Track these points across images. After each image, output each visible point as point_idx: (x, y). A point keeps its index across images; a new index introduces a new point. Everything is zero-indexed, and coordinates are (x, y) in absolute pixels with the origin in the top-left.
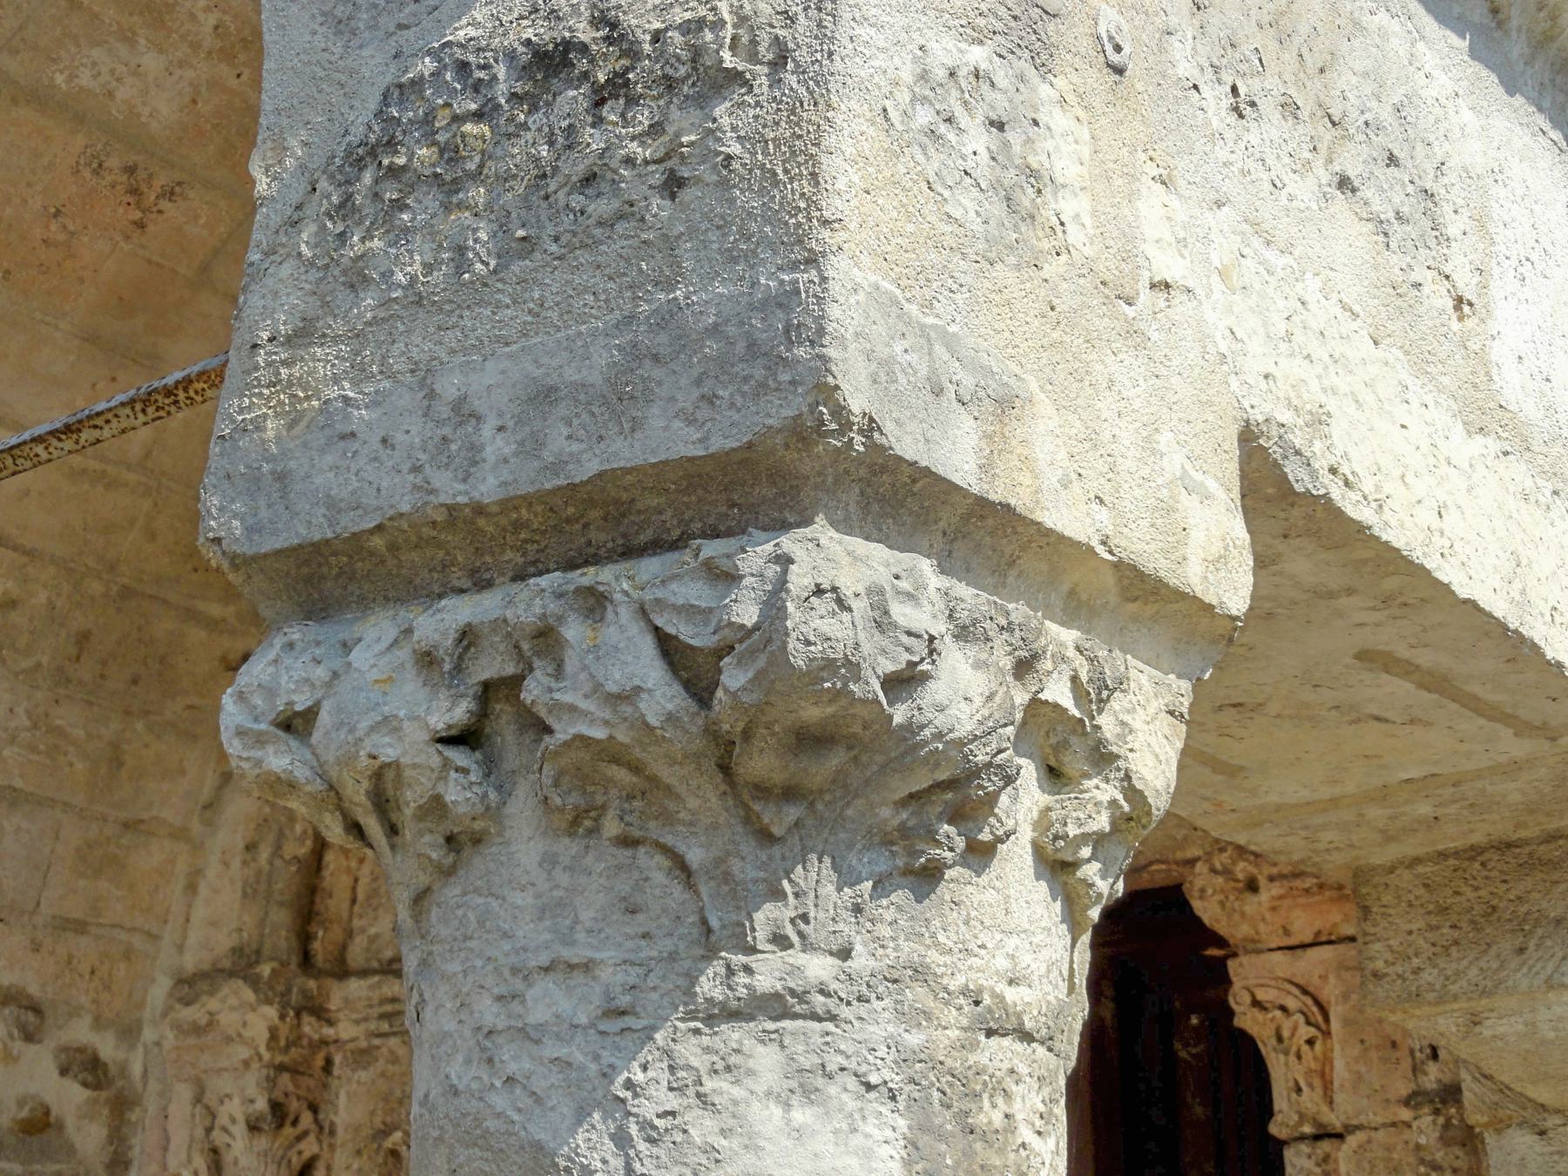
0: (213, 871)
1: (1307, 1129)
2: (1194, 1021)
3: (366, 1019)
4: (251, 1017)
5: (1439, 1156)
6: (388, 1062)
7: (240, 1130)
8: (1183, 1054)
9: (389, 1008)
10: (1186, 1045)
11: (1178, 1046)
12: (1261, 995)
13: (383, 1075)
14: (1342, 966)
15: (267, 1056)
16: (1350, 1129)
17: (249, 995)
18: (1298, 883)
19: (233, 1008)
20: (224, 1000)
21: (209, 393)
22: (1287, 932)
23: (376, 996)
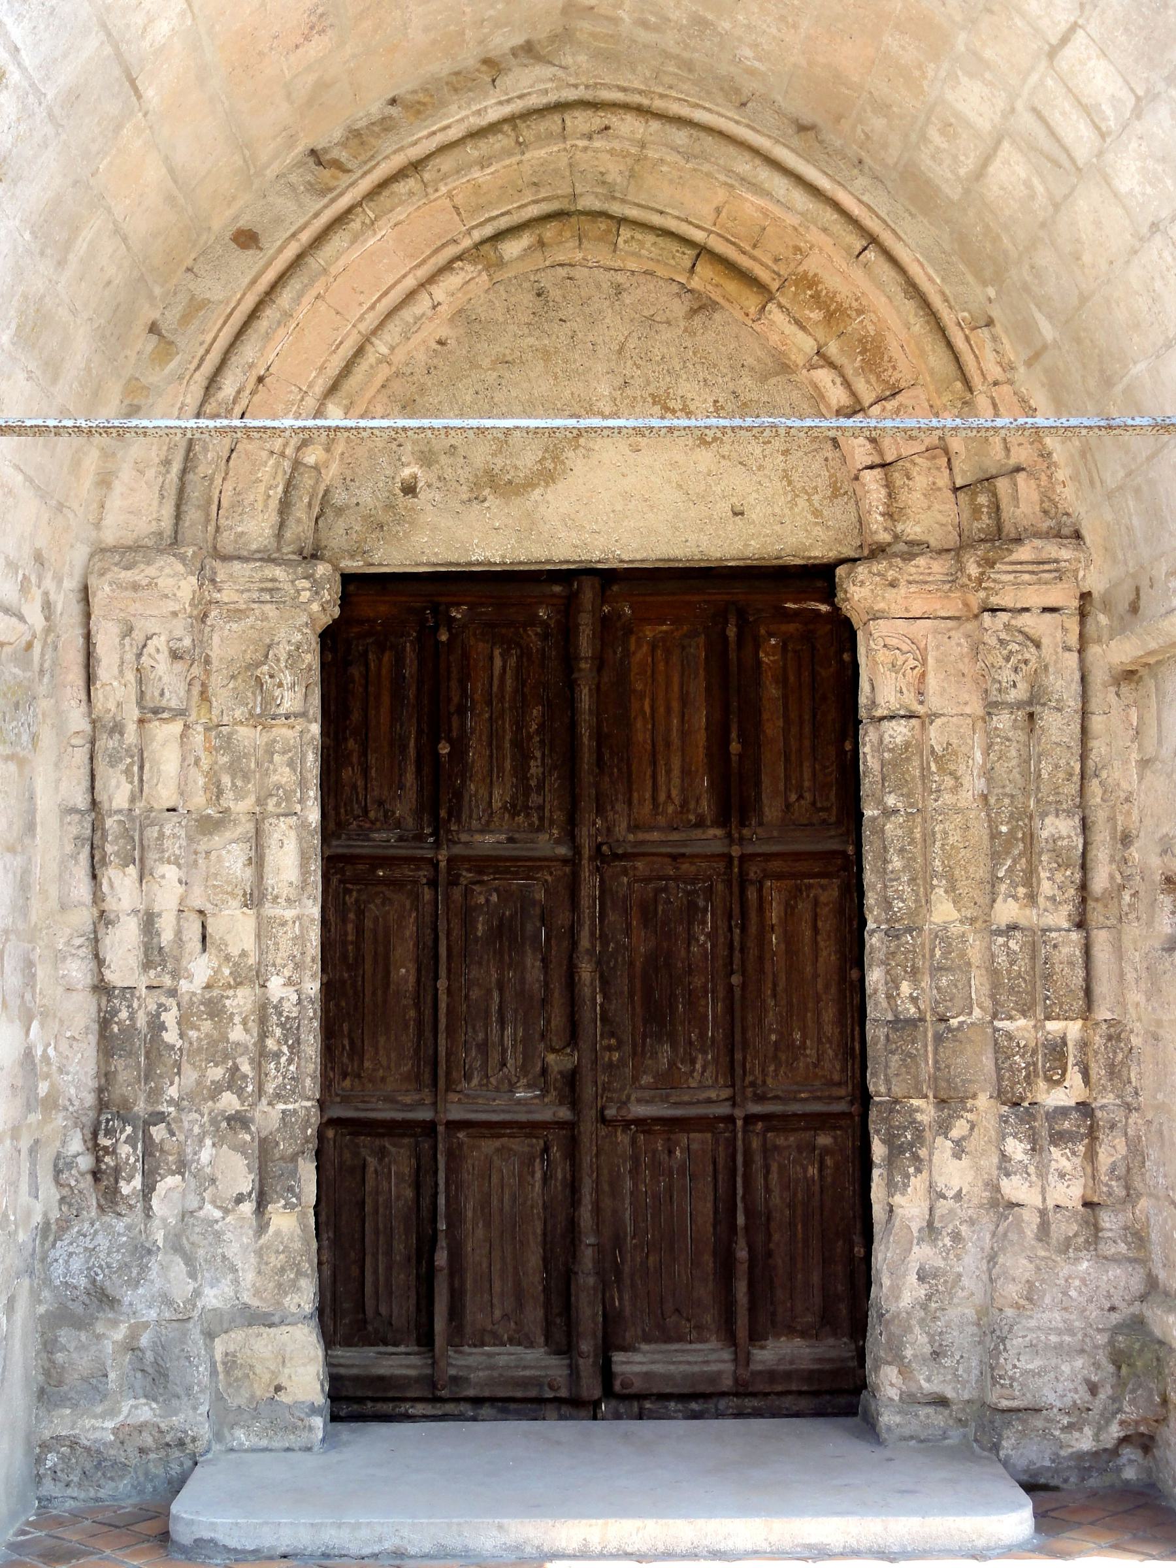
0: (126, 474)
1: (902, 713)
2: (773, 642)
3: (249, 590)
4: (183, 583)
5: (1010, 734)
6: (257, 619)
7: (164, 657)
8: (765, 660)
9: (270, 585)
10: (767, 655)
11: (762, 655)
12: (888, 641)
13: (252, 627)
14: (936, 631)
15: (189, 609)
16: (937, 715)
17: (180, 568)
18: (926, 587)
19: (169, 576)
20: (161, 569)
21: (313, 19)
22: (907, 610)
23: (258, 576)
